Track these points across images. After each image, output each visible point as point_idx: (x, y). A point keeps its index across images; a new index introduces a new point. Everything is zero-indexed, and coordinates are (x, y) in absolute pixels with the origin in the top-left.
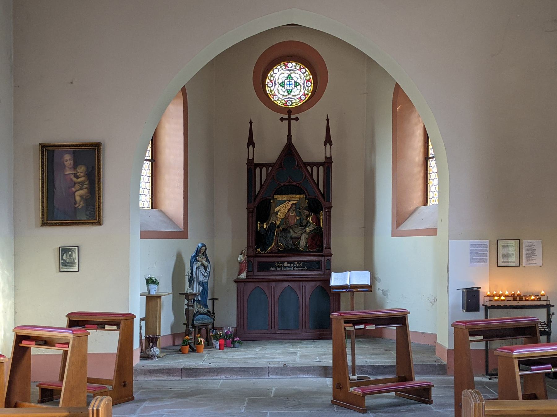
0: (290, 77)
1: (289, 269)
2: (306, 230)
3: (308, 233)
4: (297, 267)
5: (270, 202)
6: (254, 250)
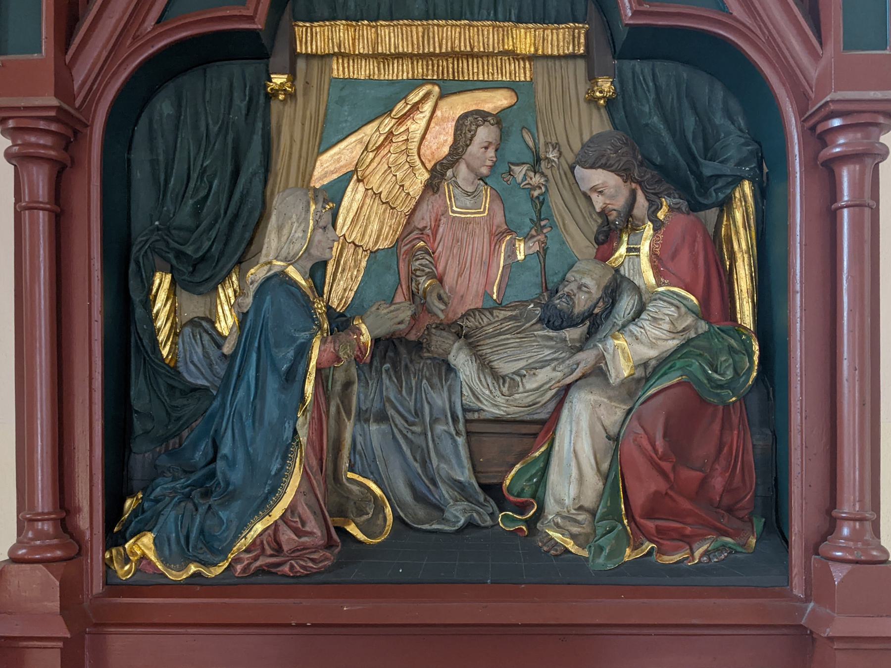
3: (623, 383)
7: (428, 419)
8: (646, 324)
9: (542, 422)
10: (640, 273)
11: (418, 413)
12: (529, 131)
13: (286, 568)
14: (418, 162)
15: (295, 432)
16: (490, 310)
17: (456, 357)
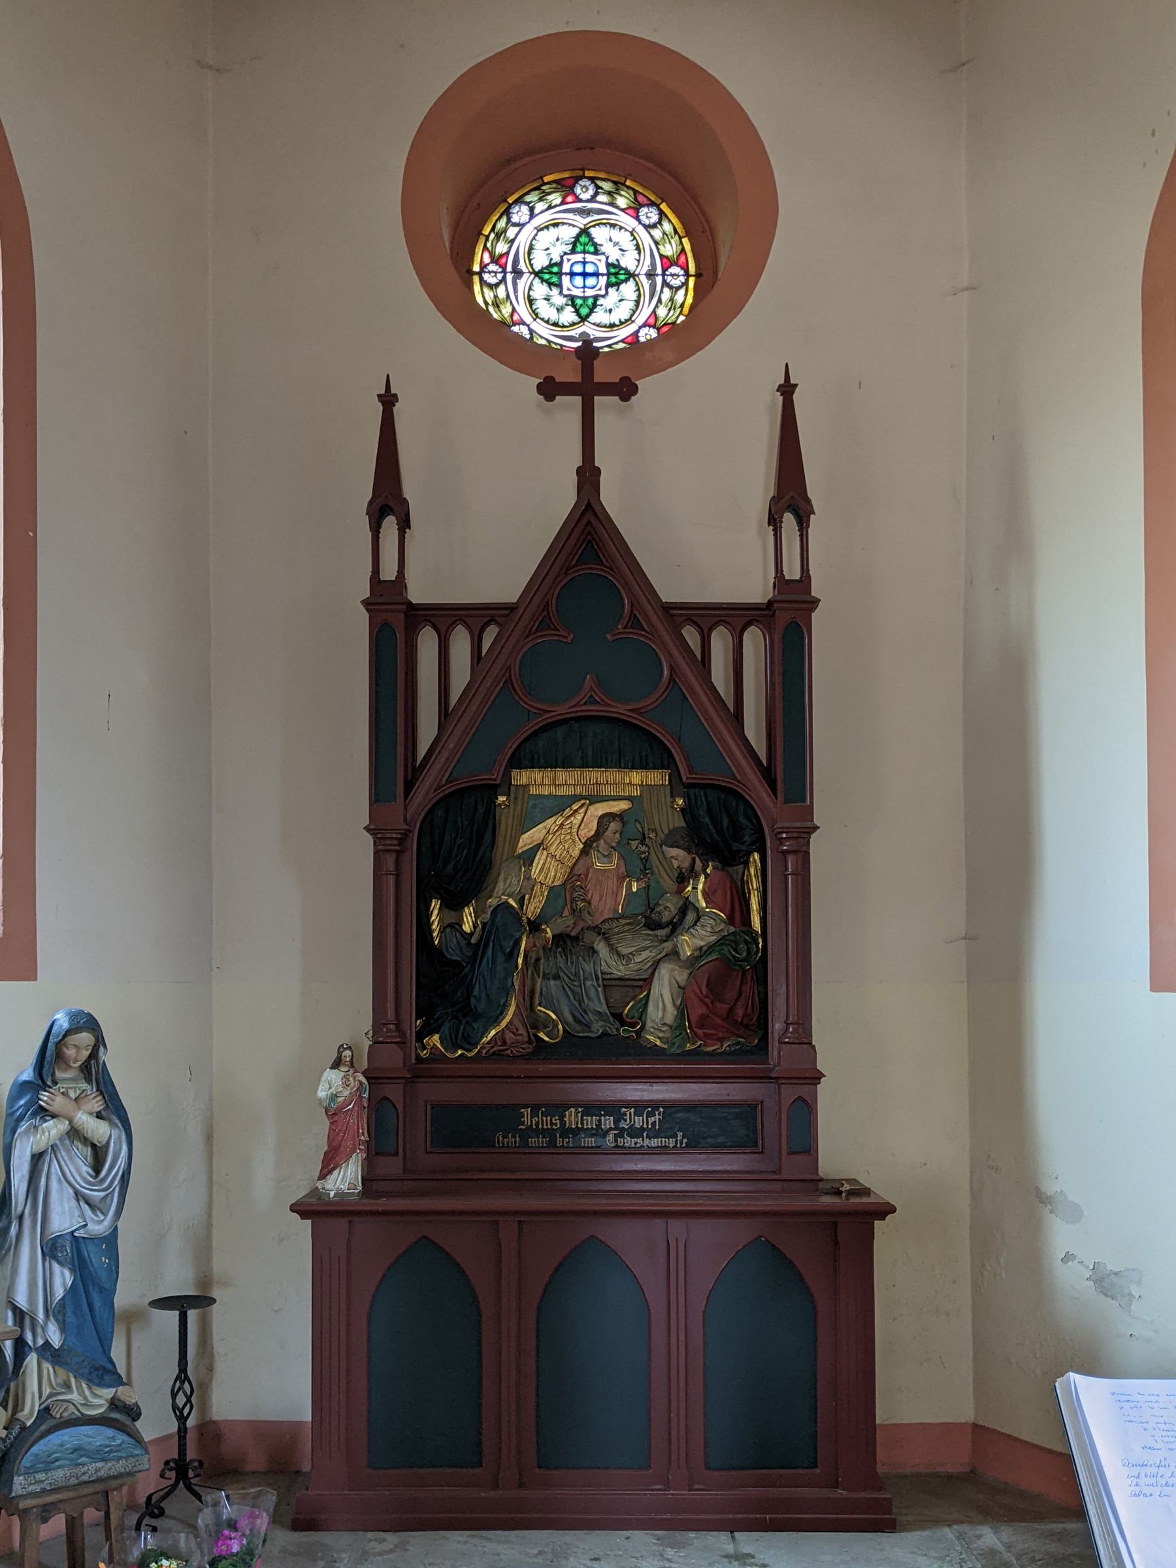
0: (585, 245)
1: (592, 1141)
2: (676, 946)
4: (635, 1133)
5: (491, 807)
7: (582, 978)
8: (698, 928)
9: (644, 980)
10: (698, 900)
11: (577, 974)
12: (639, 822)
13: (509, 1052)
14: (577, 839)
15: (513, 983)
16: (617, 919)
17: (598, 945)
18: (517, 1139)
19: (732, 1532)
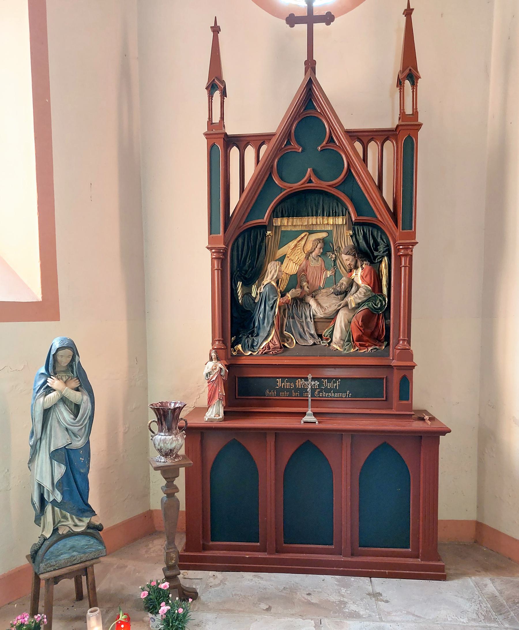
4: (328, 391)
6: (229, 345)
9: (333, 319)
13: (271, 353)
18: (275, 393)
19: (370, 578)
